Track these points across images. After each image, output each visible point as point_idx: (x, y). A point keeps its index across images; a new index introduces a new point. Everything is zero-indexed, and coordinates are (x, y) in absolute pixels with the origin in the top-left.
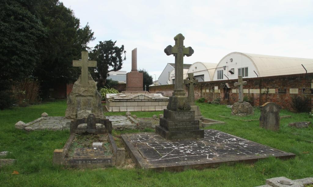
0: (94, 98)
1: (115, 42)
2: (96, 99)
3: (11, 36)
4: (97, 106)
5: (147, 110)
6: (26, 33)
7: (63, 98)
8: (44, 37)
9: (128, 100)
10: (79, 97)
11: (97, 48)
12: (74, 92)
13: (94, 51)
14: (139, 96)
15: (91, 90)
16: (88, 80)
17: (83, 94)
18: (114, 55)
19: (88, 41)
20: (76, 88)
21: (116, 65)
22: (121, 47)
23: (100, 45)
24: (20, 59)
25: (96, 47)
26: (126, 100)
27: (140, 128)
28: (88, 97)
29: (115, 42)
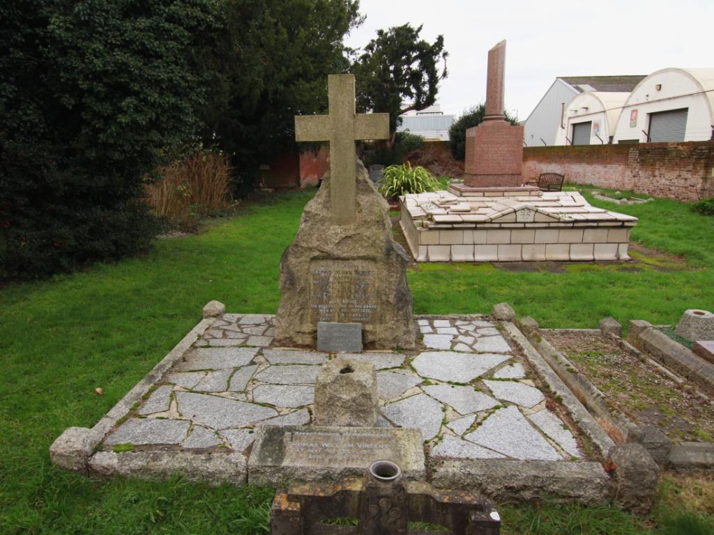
0: (380, 265)
1: (420, 29)
2: (389, 271)
3: (109, 33)
4: (392, 299)
5: (541, 257)
6: (154, 18)
7: (292, 188)
8: (209, 26)
9: (478, 226)
10: (322, 263)
11: (372, 49)
12: (304, 245)
13: (364, 57)
14: (515, 212)
15: (368, 233)
16: (357, 194)
17: (337, 253)
18: (415, 66)
19: (345, 30)
20: (311, 229)
21: (420, 92)
22: (436, 41)
23: (378, 40)
24: (145, 109)
25: (370, 47)
26: (474, 226)
27: (628, 494)
28: (359, 263)
29: (420, 29)
